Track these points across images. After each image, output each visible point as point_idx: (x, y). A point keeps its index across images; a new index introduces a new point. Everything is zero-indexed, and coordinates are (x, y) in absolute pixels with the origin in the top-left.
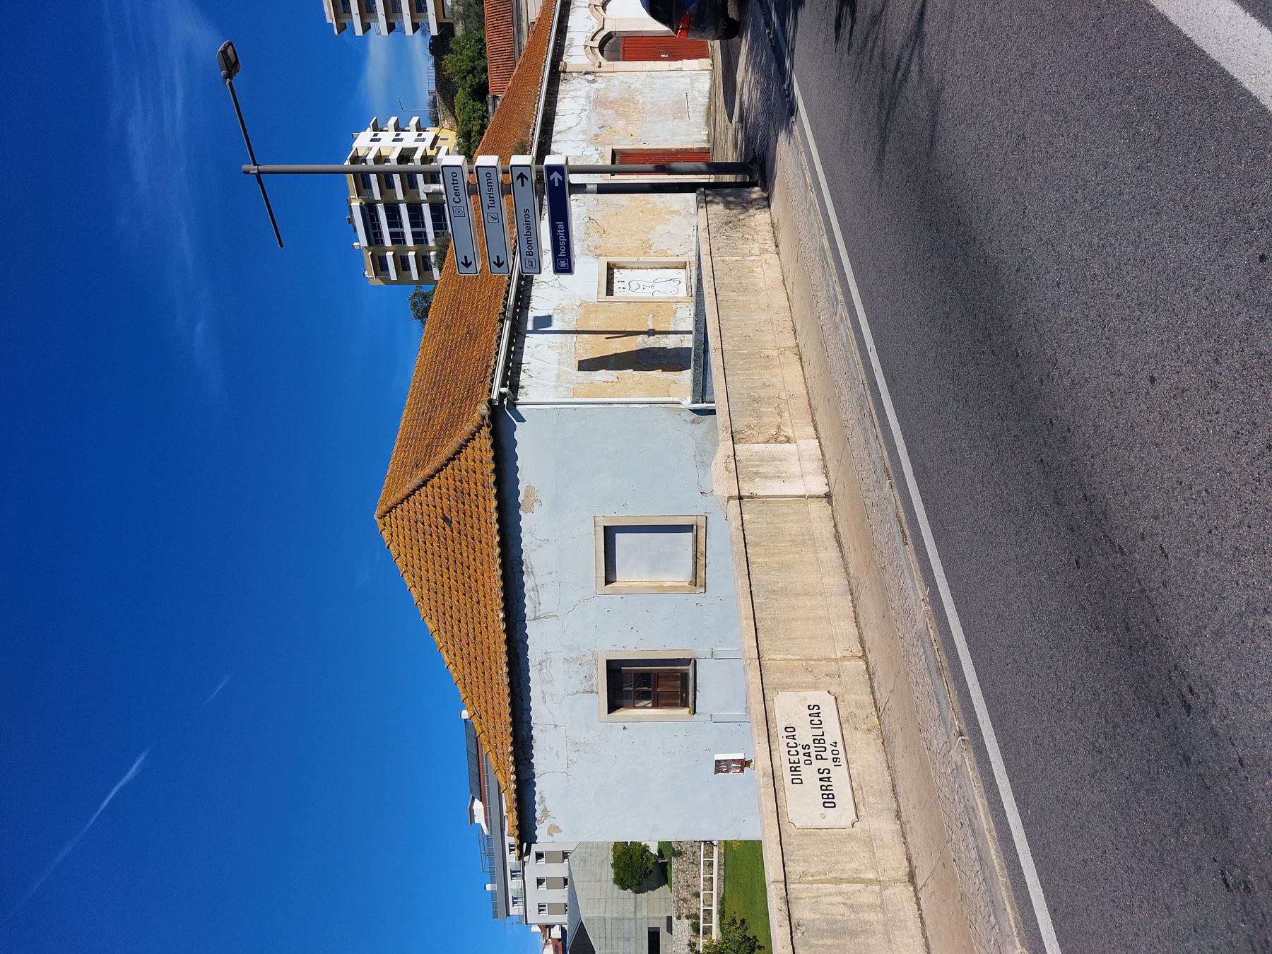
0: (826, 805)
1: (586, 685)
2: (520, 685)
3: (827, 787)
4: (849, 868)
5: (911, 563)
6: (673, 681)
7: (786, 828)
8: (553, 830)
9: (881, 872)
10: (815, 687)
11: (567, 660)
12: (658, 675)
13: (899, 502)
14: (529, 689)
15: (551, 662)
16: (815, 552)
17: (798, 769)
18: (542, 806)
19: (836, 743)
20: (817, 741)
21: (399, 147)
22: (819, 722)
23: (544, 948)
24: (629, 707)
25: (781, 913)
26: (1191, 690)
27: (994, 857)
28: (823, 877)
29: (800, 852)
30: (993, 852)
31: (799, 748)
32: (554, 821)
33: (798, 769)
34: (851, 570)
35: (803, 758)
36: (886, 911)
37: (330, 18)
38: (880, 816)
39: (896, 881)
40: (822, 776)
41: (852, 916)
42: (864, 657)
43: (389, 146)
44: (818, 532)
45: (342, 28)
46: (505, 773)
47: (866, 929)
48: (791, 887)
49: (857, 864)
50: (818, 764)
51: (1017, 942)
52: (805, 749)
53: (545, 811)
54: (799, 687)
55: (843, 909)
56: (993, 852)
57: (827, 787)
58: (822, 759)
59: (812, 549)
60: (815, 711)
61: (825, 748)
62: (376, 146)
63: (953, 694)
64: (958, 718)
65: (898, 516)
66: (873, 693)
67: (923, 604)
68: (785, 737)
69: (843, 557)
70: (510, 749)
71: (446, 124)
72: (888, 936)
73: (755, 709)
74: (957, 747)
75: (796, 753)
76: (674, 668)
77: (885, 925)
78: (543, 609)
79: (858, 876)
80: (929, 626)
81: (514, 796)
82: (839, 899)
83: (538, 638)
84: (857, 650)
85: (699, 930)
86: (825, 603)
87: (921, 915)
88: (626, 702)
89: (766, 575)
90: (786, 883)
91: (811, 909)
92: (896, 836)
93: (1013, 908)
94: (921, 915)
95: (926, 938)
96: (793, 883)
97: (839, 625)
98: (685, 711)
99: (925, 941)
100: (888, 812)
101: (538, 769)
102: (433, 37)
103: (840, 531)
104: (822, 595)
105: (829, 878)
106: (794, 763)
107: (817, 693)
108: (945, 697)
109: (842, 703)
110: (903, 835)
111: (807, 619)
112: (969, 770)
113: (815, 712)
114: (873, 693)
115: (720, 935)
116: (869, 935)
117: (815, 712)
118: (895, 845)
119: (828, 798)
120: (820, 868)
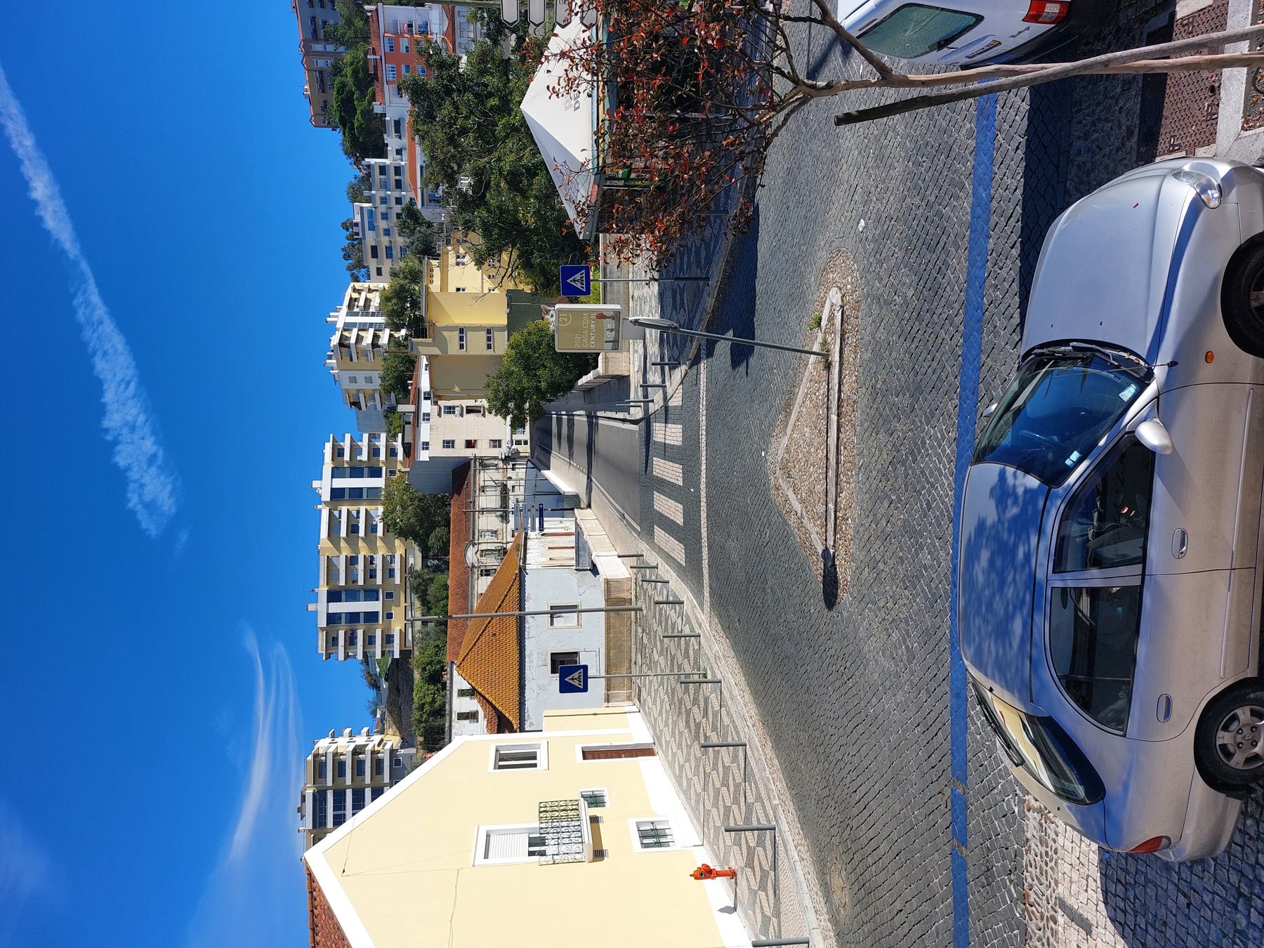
8: (531, 724)
21: (352, 746)
37: (322, 648)
43: (344, 745)
45: (328, 656)
62: (334, 746)
71: (390, 731)
78: (531, 635)
83: (529, 644)
102: (393, 660)
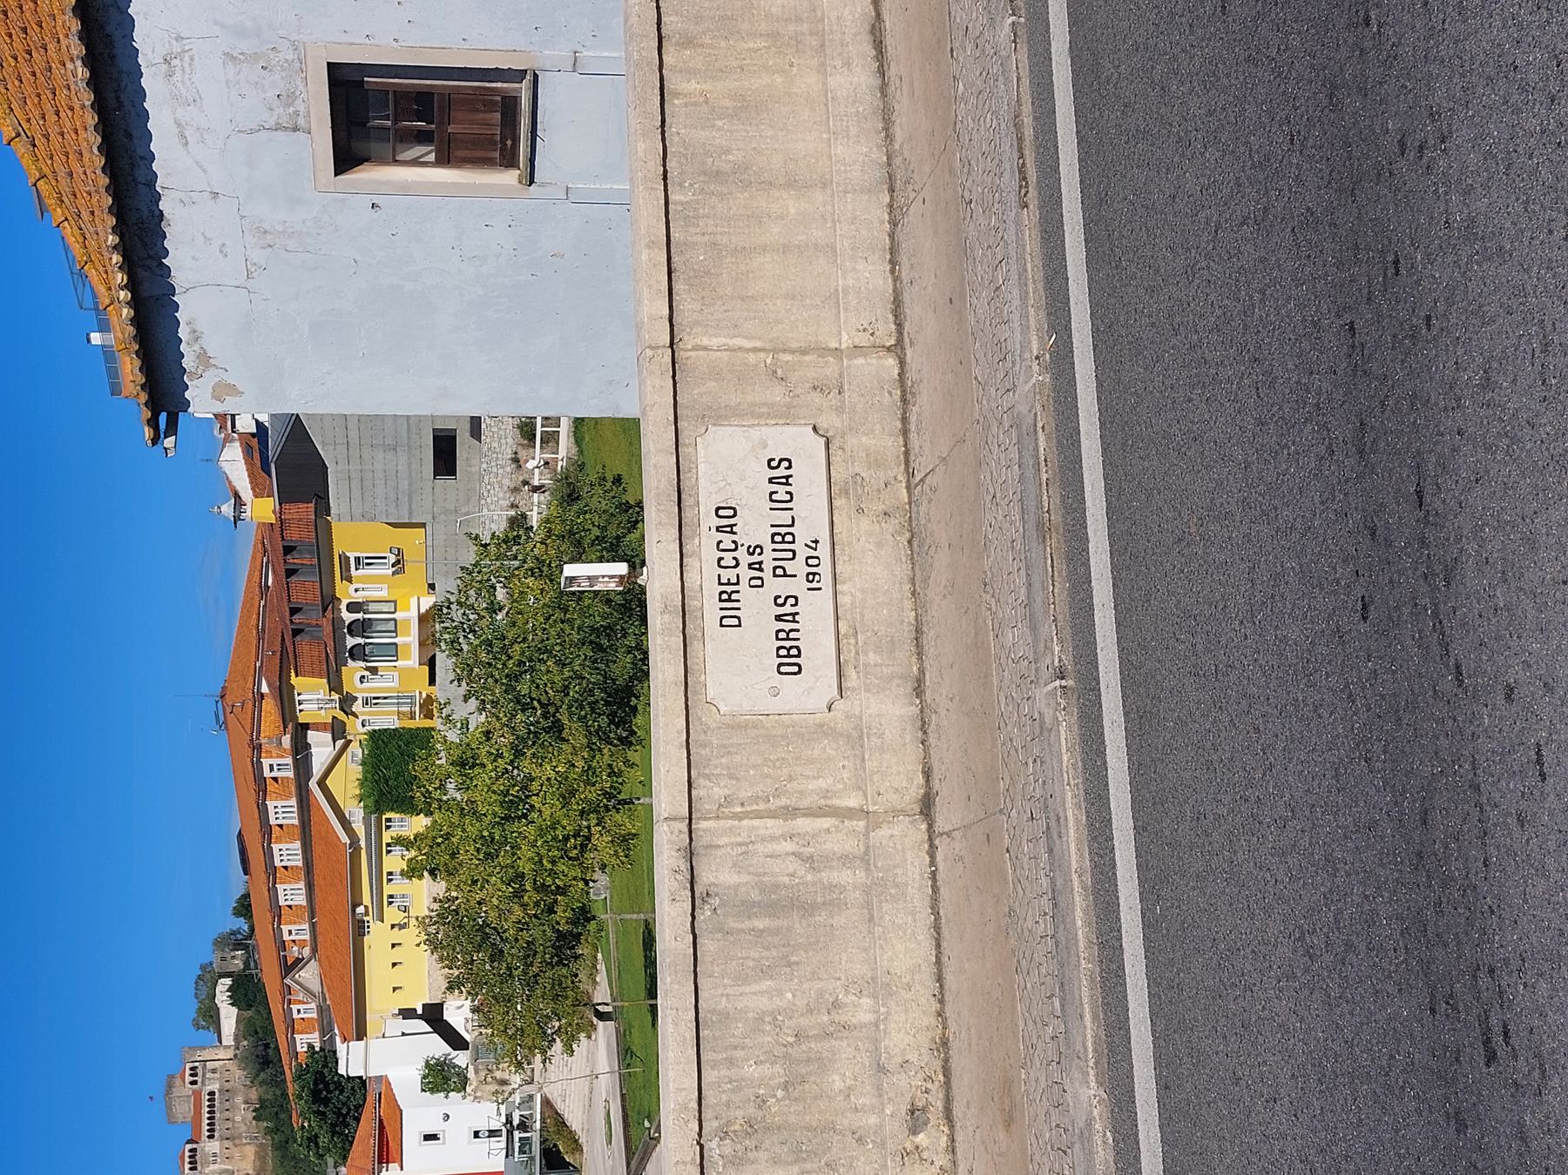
0: (783, 669)
1: (282, 114)
2: (120, 106)
3: (783, 537)
4: (813, 787)
5: (1028, 257)
6: (485, 112)
7: (700, 714)
9: (873, 797)
10: (786, 415)
11: (233, 58)
12: (448, 99)
13: (1026, 81)
14: (145, 116)
15: (192, 59)
16: (822, 69)
17: (734, 596)
18: (196, 347)
19: (816, 542)
20: (778, 538)
22: (788, 497)
23: (224, 447)
24: (383, 161)
25: (677, 876)
26: (1506, 1034)
27: (1079, 923)
28: (762, 806)
29: (723, 760)
30: (1079, 914)
31: (741, 554)
32: (224, 376)
33: (734, 596)
34: (899, 134)
35: (745, 573)
36: (872, 867)
38: (883, 690)
39: (896, 812)
40: (781, 611)
41: (809, 877)
42: (898, 348)
44: (833, 15)
46: (106, 272)
47: (833, 900)
48: (701, 825)
49: (830, 781)
50: (782, 587)
51: (1092, 1078)
52: (753, 554)
53: (204, 358)
54: (753, 415)
55: (792, 865)
56: (1079, 914)
57: (783, 537)
58: (785, 575)
59: (815, 62)
60: (782, 472)
61: (794, 552)
63: (1061, 589)
64: (1061, 641)
65: (1018, 126)
66: (905, 432)
67: (1036, 368)
68: (714, 530)
69: (883, 88)
70: (112, 239)
72: (870, 910)
73: (655, 466)
74: (1048, 693)
75: (734, 563)
76: (487, 85)
77: (867, 890)
79: (829, 802)
80: (1040, 425)
81: (131, 330)
82: (788, 846)
84: (886, 332)
85: (534, 435)
86: (829, 208)
87: (934, 874)
88: (375, 147)
89: (703, 128)
90: (690, 819)
91: (734, 865)
92: (909, 727)
93: (1095, 1017)
94: (934, 874)
95: (937, 914)
96: (706, 819)
97: (854, 269)
98: (510, 177)
99: (935, 919)
100: (899, 681)
101: (179, 278)
103: (886, 16)
104: (825, 185)
105: (773, 807)
106: (729, 583)
107: (790, 430)
108: (1044, 588)
109: (840, 452)
110: (923, 726)
111: (786, 249)
112: (1064, 750)
113: (780, 471)
114: (905, 432)
115: (574, 450)
116: (836, 910)
117: (780, 471)
118: (904, 745)
119: (789, 656)
120: (758, 789)
